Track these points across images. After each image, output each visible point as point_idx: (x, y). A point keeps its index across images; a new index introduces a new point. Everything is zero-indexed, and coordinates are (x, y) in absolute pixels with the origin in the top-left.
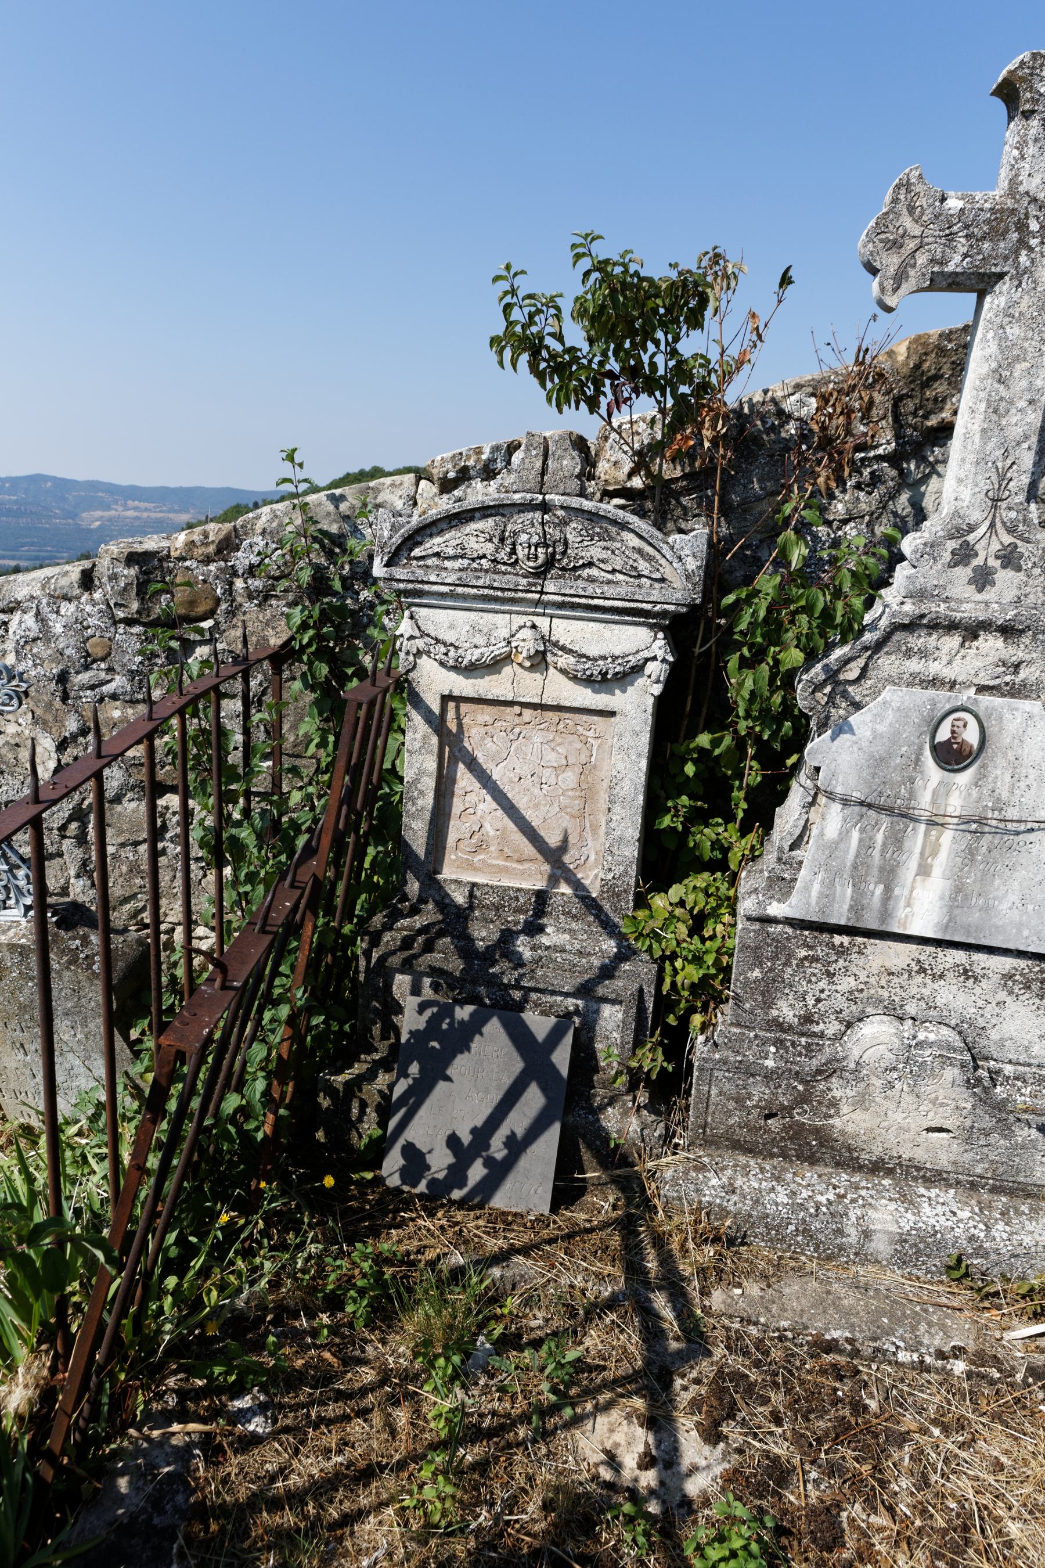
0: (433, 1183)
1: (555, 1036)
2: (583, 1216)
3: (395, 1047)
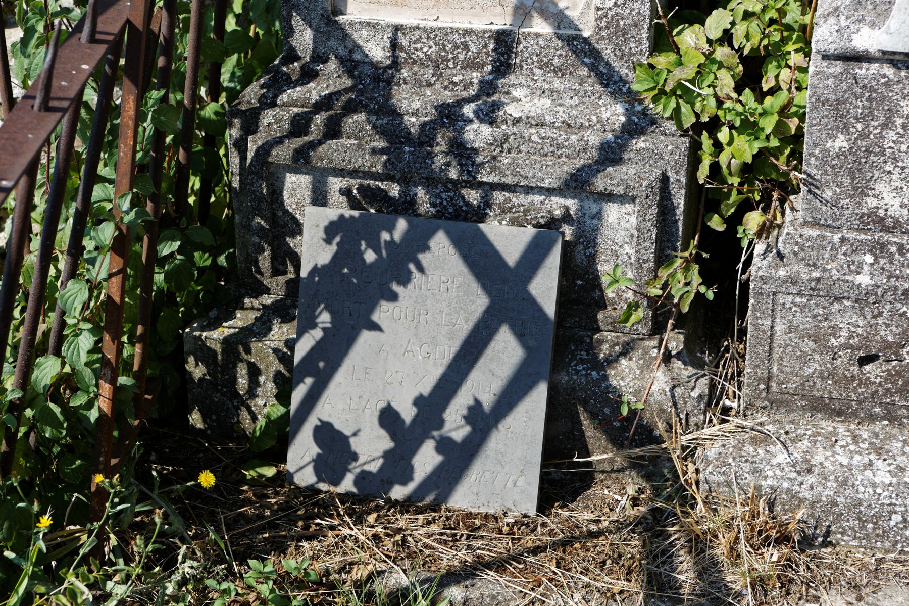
0: (363, 478)
1: (533, 257)
2: (587, 515)
3: (293, 286)
